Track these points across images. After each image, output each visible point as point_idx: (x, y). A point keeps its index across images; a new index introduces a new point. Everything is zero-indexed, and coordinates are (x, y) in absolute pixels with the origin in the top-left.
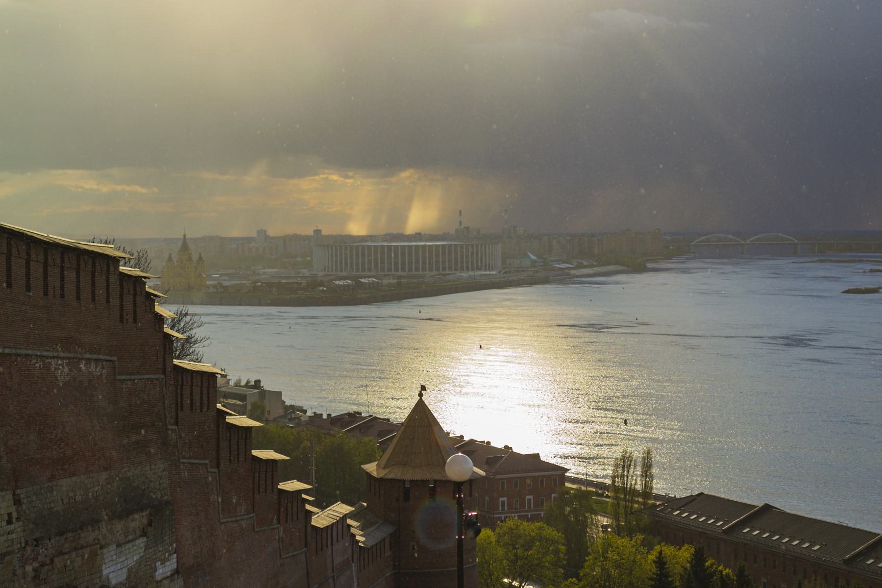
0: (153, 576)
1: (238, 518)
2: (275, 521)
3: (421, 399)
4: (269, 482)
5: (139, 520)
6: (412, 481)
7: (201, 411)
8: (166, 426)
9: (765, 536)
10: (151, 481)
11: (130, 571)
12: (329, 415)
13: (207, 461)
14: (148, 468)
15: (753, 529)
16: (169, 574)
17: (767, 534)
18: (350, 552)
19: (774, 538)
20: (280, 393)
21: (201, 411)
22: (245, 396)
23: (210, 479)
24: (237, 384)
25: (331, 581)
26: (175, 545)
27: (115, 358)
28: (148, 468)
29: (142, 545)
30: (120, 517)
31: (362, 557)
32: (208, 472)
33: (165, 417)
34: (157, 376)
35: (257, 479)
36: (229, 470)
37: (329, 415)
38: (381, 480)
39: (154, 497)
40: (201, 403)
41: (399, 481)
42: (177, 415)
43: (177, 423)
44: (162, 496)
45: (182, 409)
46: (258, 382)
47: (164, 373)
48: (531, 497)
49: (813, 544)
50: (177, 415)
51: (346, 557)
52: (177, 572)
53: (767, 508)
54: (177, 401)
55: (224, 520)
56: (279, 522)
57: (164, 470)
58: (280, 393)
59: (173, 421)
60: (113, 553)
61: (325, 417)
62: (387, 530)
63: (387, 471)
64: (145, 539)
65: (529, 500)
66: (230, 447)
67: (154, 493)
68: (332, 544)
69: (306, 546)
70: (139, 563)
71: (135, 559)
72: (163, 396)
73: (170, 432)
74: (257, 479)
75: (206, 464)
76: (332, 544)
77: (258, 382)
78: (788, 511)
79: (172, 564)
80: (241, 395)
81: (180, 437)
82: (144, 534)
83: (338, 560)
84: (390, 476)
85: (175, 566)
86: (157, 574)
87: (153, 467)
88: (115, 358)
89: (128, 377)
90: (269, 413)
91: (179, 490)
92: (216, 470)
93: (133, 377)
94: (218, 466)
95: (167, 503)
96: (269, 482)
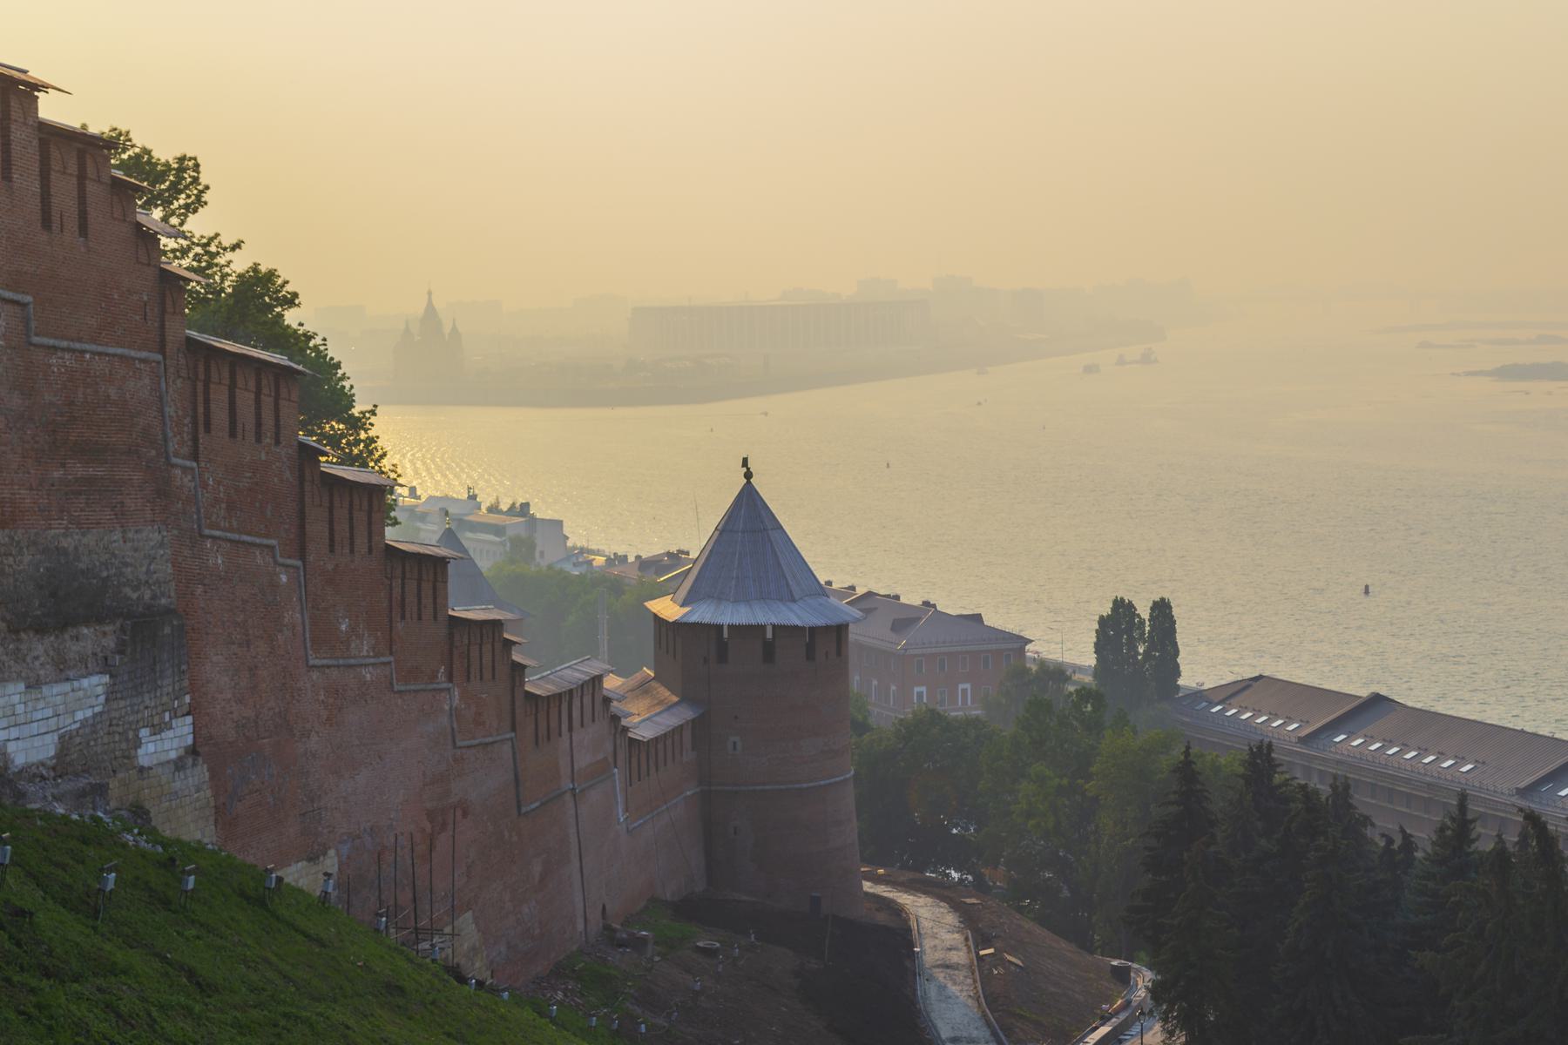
0: (129, 756)
1: (352, 661)
2: (442, 676)
3: (749, 482)
4: (427, 601)
5: (90, 639)
6: (731, 627)
7: (259, 440)
8: (167, 458)
9: (1373, 748)
10: (126, 565)
11: (65, 742)
12: (638, 557)
13: (273, 542)
14: (117, 536)
15: (1351, 735)
16: (173, 755)
17: (1378, 745)
18: (609, 747)
19: (1390, 752)
20: (559, 523)
21: (259, 440)
22: (504, 527)
23: (284, 578)
24: (493, 509)
25: (568, 797)
26: (187, 699)
27: (29, 299)
28: (117, 536)
29: (100, 690)
30: (41, 630)
31: (634, 760)
32: (276, 562)
33: (165, 440)
34: (144, 354)
35: (397, 591)
36: (330, 567)
37: (638, 557)
38: (678, 626)
39: (135, 596)
40: (259, 424)
41: (708, 626)
42: (195, 440)
43: (195, 456)
44: (154, 597)
45: (208, 429)
46: (526, 506)
47: (162, 350)
48: (968, 686)
49: (1461, 760)
50: (195, 440)
51: (600, 756)
52: (193, 751)
53: (1377, 700)
54: (195, 410)
55: (317, 662)
56: (450, 679)
57: (161, 545)
58: (559, 523)
59: (185, 450)
60: (16, 699)
61: (631, 559)
62: (686, 714)
63: (687, 609)
64: (106, 679)
65: (964, 691)
66: (331, 523)
67: (136, 588)
68: (570, 729)
69: (513, 729)
70: (92, 725)
71: (80, 716)
72: (161, 398)
73: (178, 472)
74: (397, 591)
75: (271, 548)
76: (570, 729)
77: (526, 506)
78: (1410, 704)
79: (181, 733)
80: (495, 525)
81: (205, 486)
82: (105, 667)
83: (583, 760)
84: (694, 619)
85: (190, 740)
86: (140, 752)
87: (130, 535)
88: (29, 299)
89: (65, 344)
90: (542, 553)
91: (200, 589)
92: (299, 563)
93: (77, 346)
94: (302, 554)
95: (169, 612)
96: (427, 601)
